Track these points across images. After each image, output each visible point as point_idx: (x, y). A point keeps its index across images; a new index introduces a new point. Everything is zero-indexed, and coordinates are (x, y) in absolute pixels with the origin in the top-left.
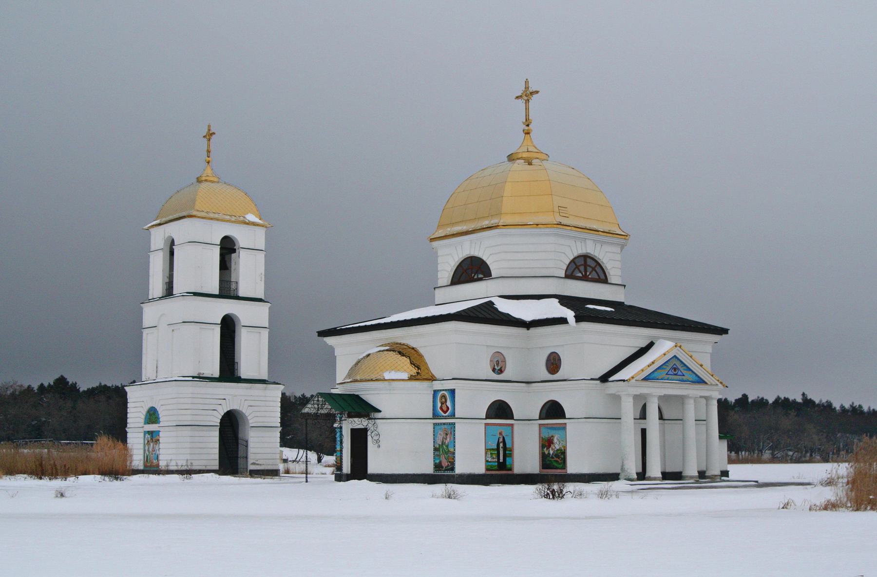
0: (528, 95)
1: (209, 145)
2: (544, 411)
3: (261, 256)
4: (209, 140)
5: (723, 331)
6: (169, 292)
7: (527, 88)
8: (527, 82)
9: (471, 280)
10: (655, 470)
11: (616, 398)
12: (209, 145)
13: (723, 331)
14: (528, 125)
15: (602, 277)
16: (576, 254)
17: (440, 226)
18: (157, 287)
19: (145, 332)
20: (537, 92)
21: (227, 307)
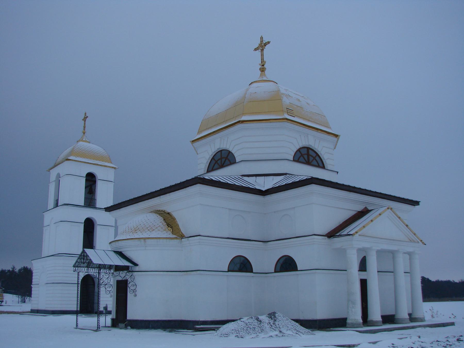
0: (262, 46)
1: (85, 124)
2: (279, 265)
3: (111, 185)
4: (85, 121)
5: (415, 203)
6: (57, 205)
7: (262, 41)
8: (262, 38)
9: (222, 166)
10: (376, 314)
11: (342, 252)
12: (85, 124)
13: (415, 203)
14: (263, 65)
15: (321, 165)
16: (301, 145)
17: (199, 133)
18: (51, 203)
19: (45, 228)
20: (269, 42)
21: (89, 213)
